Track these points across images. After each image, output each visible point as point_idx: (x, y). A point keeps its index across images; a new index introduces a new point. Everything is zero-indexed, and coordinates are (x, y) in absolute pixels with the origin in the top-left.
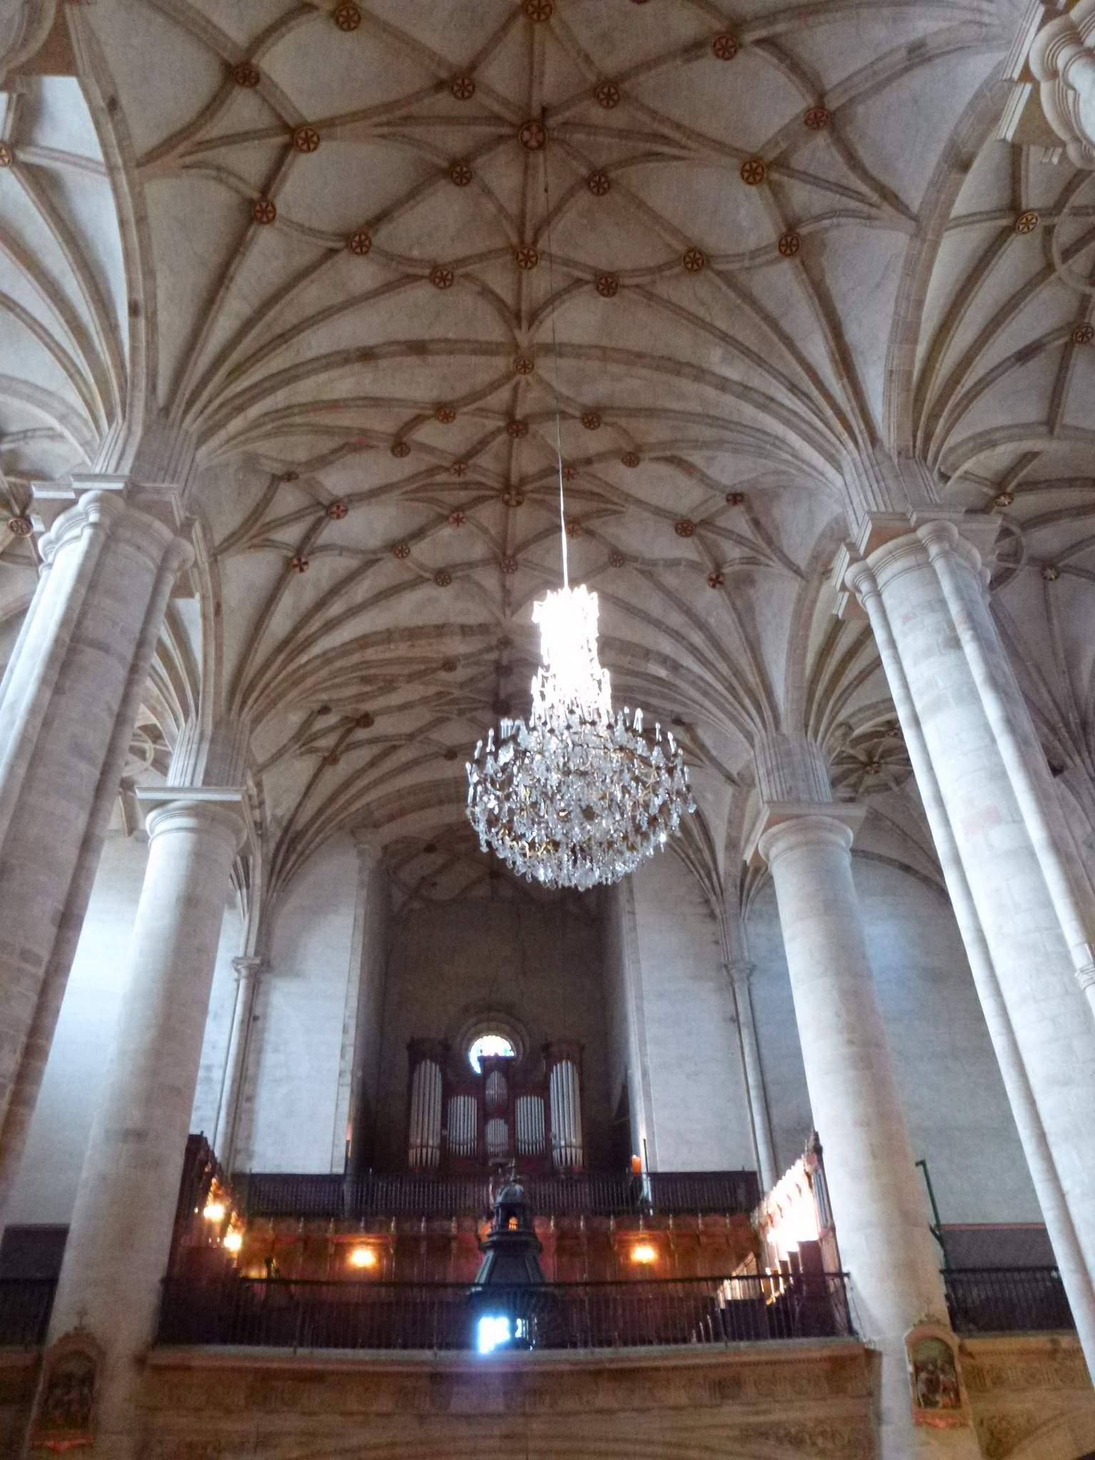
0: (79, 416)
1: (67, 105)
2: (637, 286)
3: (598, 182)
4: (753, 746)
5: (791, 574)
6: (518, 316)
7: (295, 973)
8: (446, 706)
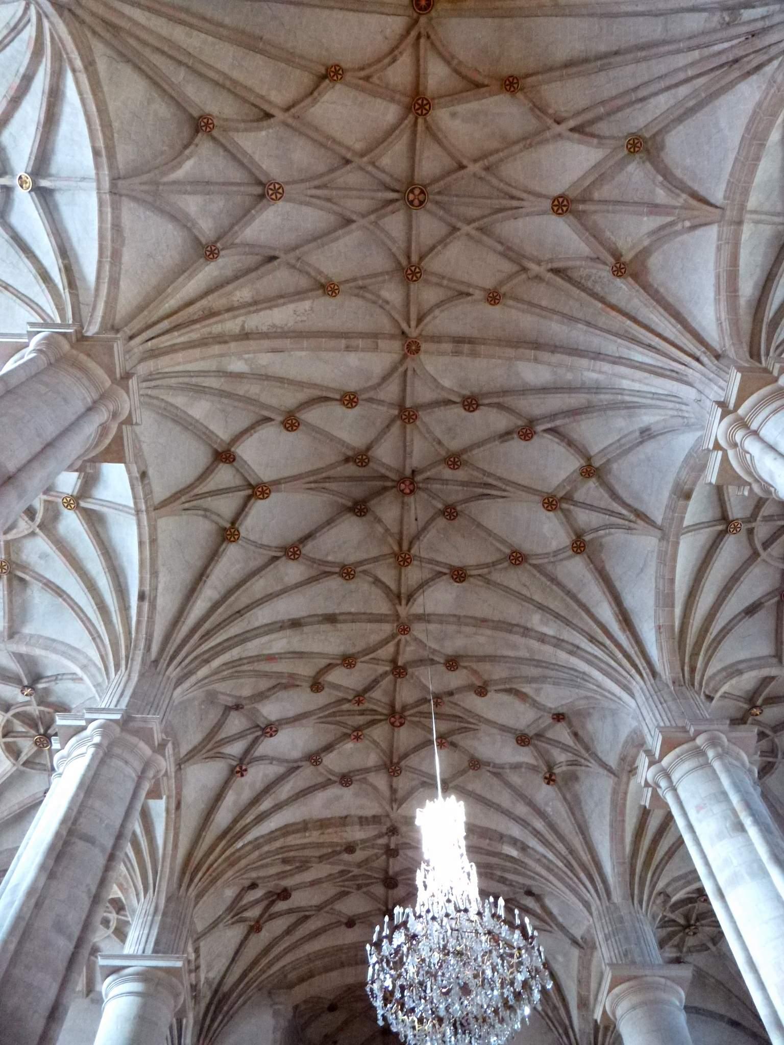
0: (95, 665)
1: (116, 481)
2: (479, 575)
3: (450, 512)
4: (591, 914)
5: (606, 772)
6: (399, 597)
8: (349, 883)
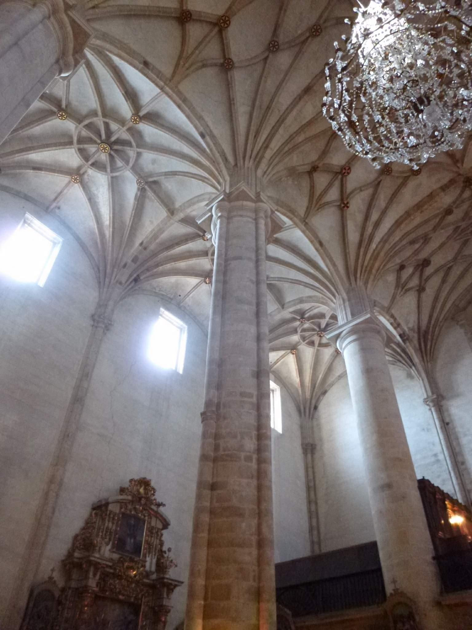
7: (457, 395)
